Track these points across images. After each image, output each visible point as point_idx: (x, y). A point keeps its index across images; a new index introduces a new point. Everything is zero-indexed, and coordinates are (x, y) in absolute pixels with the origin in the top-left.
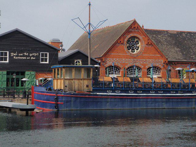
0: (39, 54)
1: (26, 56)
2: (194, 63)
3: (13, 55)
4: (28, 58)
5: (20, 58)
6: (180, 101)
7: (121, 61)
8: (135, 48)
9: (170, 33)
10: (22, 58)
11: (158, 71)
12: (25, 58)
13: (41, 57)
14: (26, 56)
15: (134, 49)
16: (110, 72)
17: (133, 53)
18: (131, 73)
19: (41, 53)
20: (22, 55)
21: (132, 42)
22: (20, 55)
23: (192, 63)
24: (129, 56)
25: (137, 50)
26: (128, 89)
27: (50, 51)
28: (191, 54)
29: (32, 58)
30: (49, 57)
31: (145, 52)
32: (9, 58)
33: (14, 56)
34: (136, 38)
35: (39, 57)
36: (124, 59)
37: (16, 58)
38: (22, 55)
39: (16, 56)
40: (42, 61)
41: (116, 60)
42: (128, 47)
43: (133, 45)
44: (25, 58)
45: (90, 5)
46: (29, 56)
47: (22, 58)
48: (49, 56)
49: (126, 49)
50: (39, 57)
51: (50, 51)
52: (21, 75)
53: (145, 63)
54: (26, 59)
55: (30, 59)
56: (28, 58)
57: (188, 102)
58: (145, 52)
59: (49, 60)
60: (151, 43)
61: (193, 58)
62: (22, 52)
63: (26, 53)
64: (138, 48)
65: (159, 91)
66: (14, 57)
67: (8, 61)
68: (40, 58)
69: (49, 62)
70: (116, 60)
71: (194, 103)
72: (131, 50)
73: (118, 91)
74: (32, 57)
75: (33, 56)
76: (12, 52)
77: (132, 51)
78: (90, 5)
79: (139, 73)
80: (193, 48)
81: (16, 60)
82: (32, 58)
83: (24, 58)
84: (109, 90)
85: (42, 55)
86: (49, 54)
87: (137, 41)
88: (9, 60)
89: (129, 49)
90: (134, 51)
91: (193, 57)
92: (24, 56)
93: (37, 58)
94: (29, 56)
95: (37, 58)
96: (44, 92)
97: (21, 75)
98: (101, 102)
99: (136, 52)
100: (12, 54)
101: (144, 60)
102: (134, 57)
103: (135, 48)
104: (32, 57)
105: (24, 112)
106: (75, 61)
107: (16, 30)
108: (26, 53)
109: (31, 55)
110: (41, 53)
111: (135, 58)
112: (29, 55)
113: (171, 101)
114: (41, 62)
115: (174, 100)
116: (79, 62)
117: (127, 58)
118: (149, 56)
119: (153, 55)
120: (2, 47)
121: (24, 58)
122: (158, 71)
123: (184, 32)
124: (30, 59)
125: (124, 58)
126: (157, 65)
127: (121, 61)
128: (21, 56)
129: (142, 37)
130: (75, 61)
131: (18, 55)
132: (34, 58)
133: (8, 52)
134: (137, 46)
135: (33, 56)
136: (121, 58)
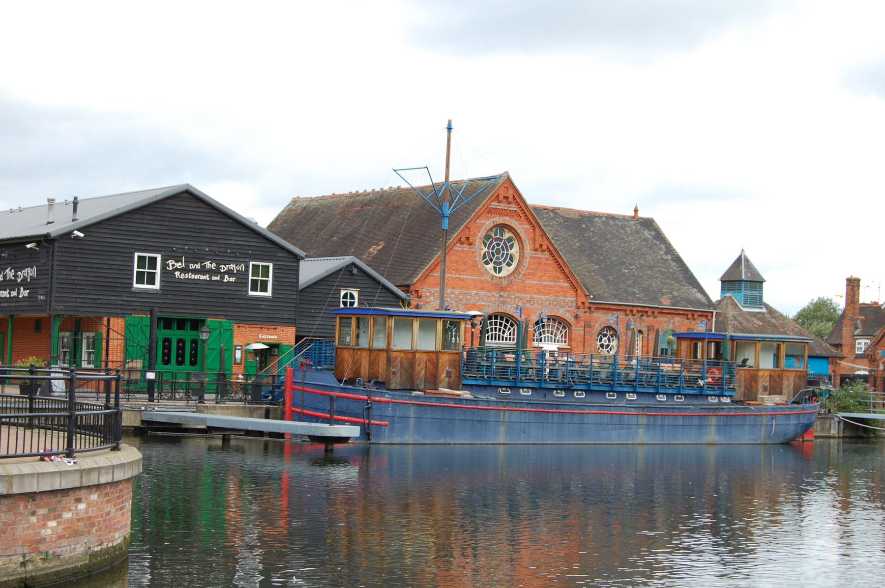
0: (247, 267)
1: (211, 272)
2: (639, 309)
3: (173, 265)
4: (214, 278)
5: (193, 277)
6: (681, 424)
7: (467, 299)
8: (504, 260)
9: (563, 217)
10: (197, 277)
11: (509, 329)
12: (207, 277)
13: (250, 277)
14: (211, 272)
15: (501, 264)
16: (543, 336)
17: (497, 275)
18: (490, 333)
19: (251, 263)
20: (198, 266)
21: (496, 239)
22: (192, 266)
23: (635, 310)
24: (488, 282)
25: (509, 265)
26: (553, 386)
27: (276, 259)
28: (629, 283)
29: (226, 278)
30: (274, 277)
31: (530, 274)
32: (162, 277)
33: (177, 269)
34: (506, 230)
35: (246, 277)
36: (474, 292)
37: (182, 276)
38: (198, 266)
39: (182, 270)
40: (254, 289)
41: (452, 293)
42: (484, 257)
43: (498, 252)
44: (207, 277)
45: (449, 129)
46: (216, 272)
47: (197, 277)
48: (274, 273)
49: (480, 262)
50: (246, 277)
51: (276, 259)
52: (191, 330)
53: (528, 305)
54: (211, 280)
55: (221, 281)
56: (214, 278)
57: (700, 426)
58: (530, 274)
59: (274, 285)
60: (548, 248)
61: (636, 294)
62: (200, 259)
63: (211, 263)
64: (511, 259)
65: (553, 389)
66: (177, 273)
67: (157, 286)
68: (247, 279)
69: (273, 292)
70: (452, 293)
71: (713, 429)
72: (491, 265)
73: (525, 392)
74: (226, 277)
75: (230, 273)
76: (172, 257)
77: (495, 269)
78: (449, 129)
79: (512, 337)
80: (630, 264)
81: (180, 281)
82: (226, 278)
83: (203, 277)
84: (580, 390)
85: (255, 267)
86: (274, 269)
87: (510, 239)
88: (162, 281)
89: (487, 263)
90: (500, 270)
91: (634, 293)
92: (203, 271)
93: (242, 276)
94: (216, 272)
95: (242, 276)
96: (332, 388)
97: (191, 330)
98: (487, 422)
99: (506, 271)
100: (171, 262)
101: (528, 296)
102: (500, 287)
103: (504, 260)
104: (226, 277)
105: (322, 447)
106: (343, 293)
107: (184, 189)
108: (211, 263)
109: (224, 268)
110: (251, 263)
111: (502, 289)
112: (218, 268)
113: (507, 419)
114: (251, 293)
115: (667, 421)
116: (352, 297)
117: (482, 289)
118: (540, 284)
119: (550, 281)
120: (143, 239)
121: (203, 277)
122: (509, 329)
123: (599, 216)
124: (221, 281)
125: (475, 288)
126: (560, 312)
127: (467, 299)
128: (195, 271)
129: (523, 228)
130: (343, 293)
131: (187, 266)
132: (232, 279)
133: (159, 257)
134: (507, 254)
135: (230, 273)
136: (467, 288)
